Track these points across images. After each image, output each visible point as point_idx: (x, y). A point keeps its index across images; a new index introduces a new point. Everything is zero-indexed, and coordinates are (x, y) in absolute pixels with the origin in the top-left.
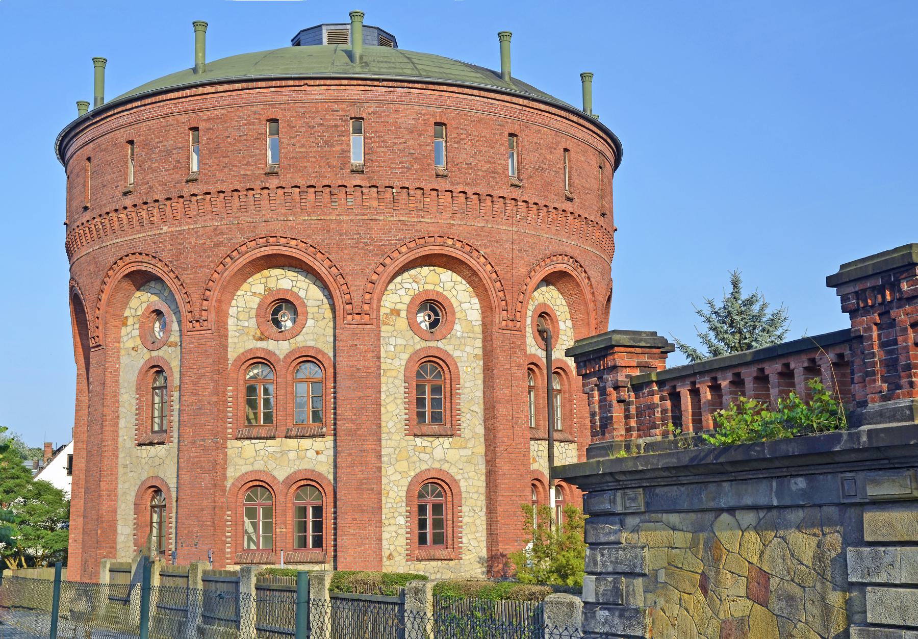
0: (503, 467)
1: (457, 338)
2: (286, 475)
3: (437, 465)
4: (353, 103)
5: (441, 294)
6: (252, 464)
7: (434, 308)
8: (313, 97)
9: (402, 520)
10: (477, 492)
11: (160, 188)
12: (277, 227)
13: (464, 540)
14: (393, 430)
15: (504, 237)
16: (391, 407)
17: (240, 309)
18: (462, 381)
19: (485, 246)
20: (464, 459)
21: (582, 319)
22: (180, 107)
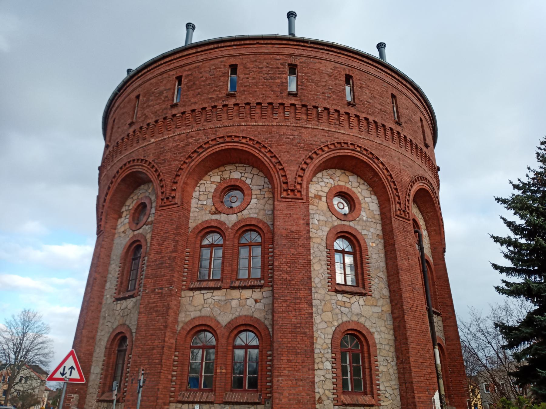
1: (363, 221)
2: (228, 320)
3: (355, 318)
4: (291, 55)
5: (351, 190)
6: (200, 311)
8: (263, 50)
9: (328, 365)
10: (388, 344)
11: (152, 115)
13: (382, 387)
15: (394, 153)
17: (201, 193)
18: (369, 253)
19: (382, 157)
20: (376, 315)
21: (435, 230)
22: (172, 66)
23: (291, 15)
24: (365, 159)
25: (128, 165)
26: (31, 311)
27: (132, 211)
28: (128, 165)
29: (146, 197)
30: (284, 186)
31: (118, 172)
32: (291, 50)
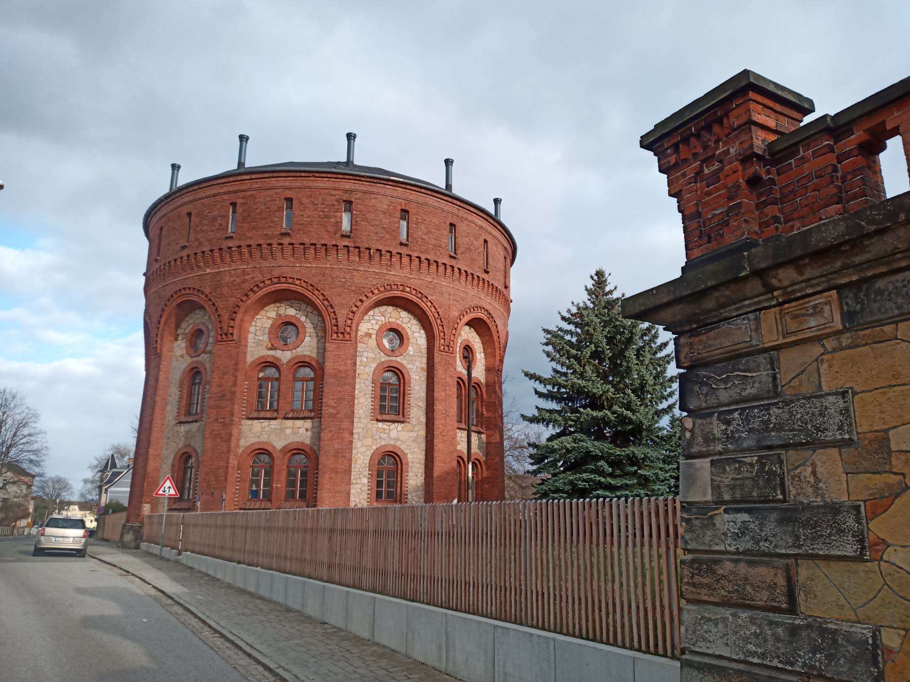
0: (438, 445)
3: (392, 442)
4: (346, 191)
7: (398, 333)
9: (365, 481)
12: (287, 271)
14: (362, 416)
15: (444, 290)
16: (362, 400)
19: (432, 295)
22: (225, 189)
23: (351, 137)
24: (414, 298)
25: (183, 292)
26: (8, 390)
27: (189, 336)
28: (183, 292)
29: (204, 324)
30: (335, 328)
31: (172, 296)
32: (348, 180)
